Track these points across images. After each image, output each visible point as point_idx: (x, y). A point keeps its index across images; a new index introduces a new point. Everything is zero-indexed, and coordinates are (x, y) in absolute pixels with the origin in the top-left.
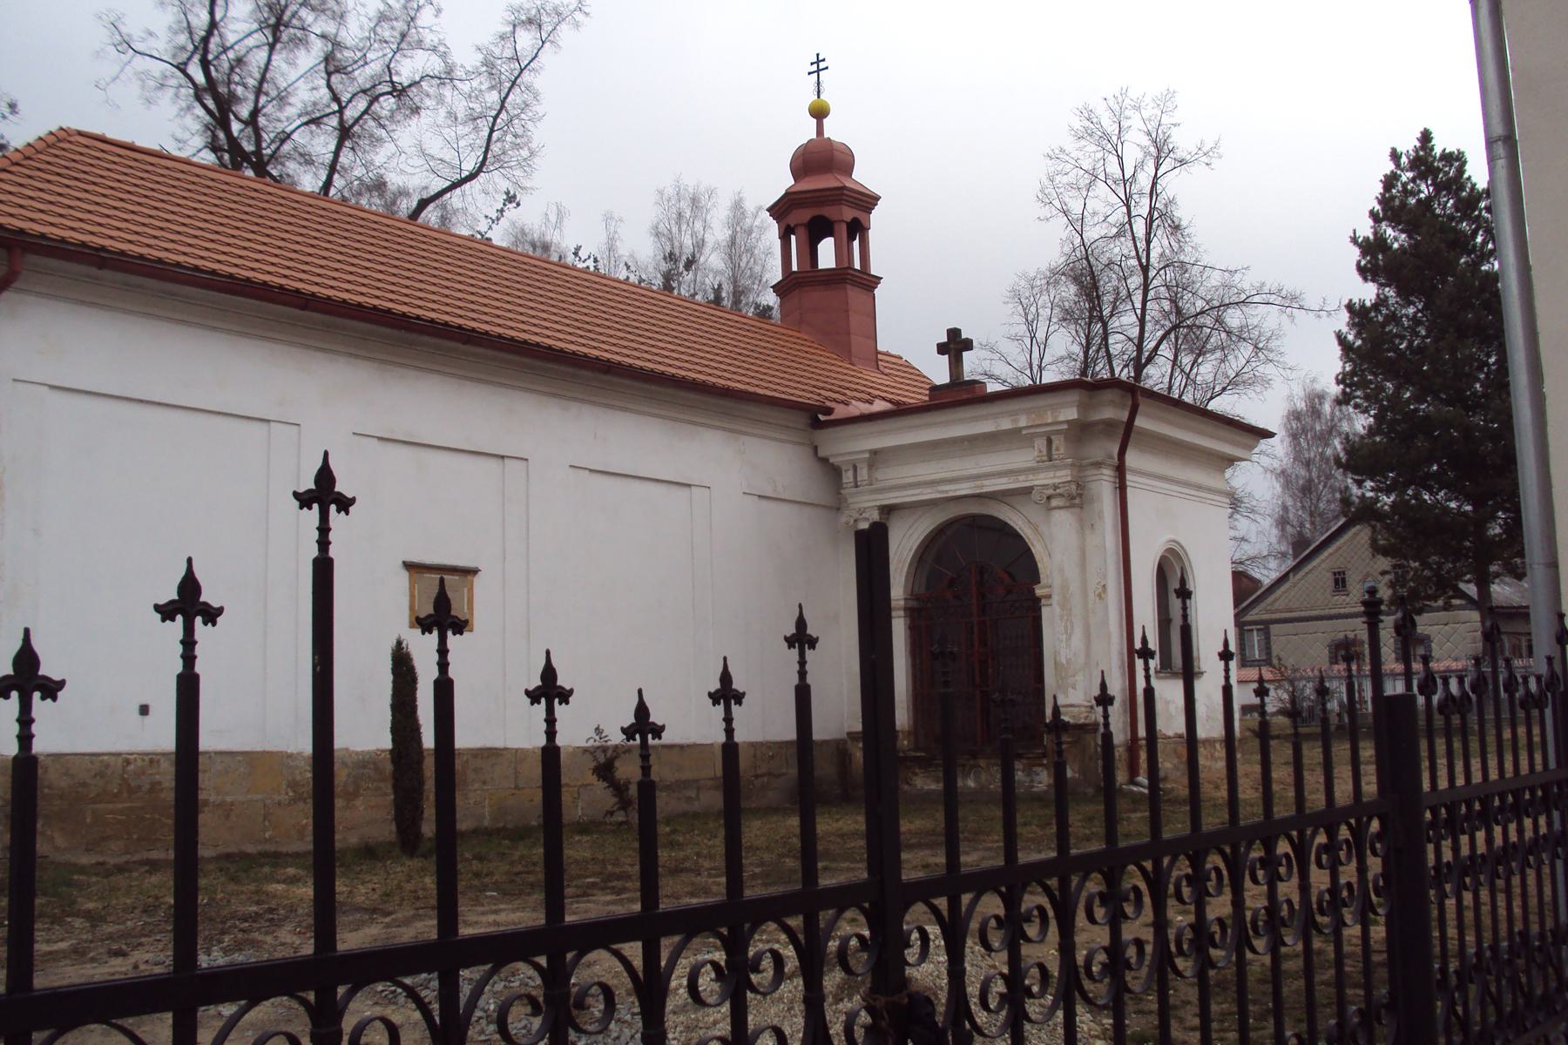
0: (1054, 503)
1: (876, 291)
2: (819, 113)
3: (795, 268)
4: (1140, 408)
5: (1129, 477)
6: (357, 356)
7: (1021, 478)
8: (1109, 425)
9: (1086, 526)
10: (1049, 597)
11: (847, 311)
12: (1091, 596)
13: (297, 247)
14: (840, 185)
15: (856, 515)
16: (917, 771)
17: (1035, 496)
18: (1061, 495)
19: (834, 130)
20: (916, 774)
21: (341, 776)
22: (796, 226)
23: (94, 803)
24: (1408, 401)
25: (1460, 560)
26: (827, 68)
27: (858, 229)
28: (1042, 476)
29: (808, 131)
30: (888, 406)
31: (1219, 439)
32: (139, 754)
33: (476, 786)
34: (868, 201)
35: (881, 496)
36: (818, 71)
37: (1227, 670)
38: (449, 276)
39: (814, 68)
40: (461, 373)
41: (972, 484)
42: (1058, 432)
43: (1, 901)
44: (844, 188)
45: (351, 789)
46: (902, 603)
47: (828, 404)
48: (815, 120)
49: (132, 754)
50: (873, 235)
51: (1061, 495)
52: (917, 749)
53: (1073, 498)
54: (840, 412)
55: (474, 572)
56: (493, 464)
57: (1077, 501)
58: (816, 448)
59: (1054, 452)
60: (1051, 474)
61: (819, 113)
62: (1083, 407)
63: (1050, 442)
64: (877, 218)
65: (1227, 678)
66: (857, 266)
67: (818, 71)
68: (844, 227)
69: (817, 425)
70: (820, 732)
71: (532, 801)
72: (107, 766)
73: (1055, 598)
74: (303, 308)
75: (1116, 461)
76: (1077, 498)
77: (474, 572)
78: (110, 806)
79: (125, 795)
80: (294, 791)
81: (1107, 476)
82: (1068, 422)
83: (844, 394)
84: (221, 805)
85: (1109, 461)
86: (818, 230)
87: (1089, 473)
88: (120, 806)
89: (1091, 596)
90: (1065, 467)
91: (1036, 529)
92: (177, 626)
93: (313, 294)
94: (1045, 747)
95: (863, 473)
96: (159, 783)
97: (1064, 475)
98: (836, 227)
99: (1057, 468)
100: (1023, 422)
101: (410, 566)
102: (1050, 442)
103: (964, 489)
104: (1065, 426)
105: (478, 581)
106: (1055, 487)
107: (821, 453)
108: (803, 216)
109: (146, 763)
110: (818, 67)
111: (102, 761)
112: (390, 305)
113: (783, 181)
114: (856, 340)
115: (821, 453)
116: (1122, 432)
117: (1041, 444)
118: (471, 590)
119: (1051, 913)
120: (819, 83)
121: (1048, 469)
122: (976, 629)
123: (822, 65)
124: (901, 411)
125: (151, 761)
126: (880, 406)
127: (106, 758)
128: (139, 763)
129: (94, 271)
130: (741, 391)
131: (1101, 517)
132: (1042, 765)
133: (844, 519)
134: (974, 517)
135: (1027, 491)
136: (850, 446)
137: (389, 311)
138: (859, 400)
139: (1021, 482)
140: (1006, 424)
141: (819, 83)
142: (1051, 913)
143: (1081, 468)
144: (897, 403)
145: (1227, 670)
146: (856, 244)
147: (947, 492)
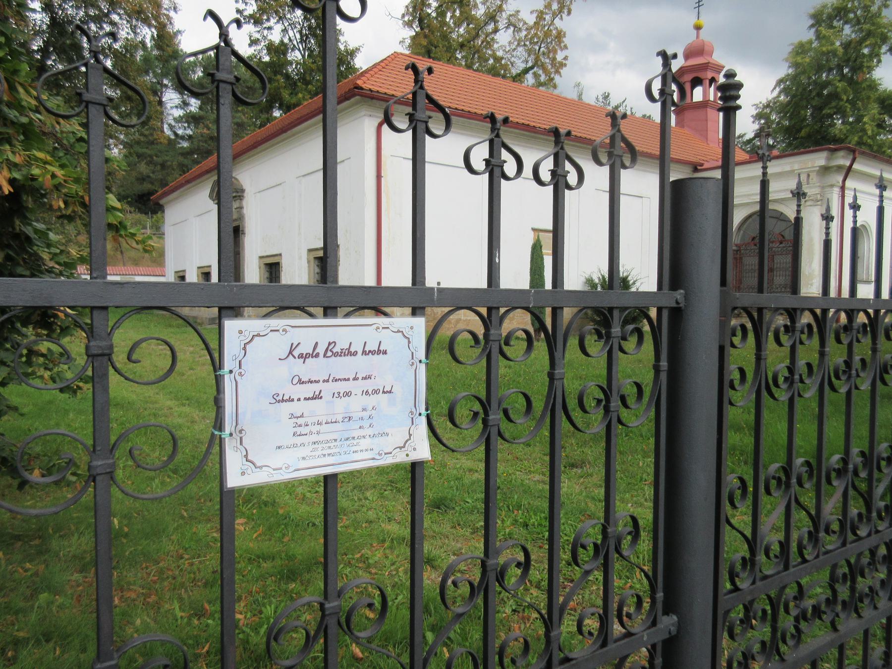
2: (698, 28)
6: (526, 147)
8: (839, 168)
11: (707, 120)
25: (847, 46)
36: (699, 6)
48: (695, 32)
54: (706, 165)
57: (819, 203)
59: (810, 180)
61: (698, 28)
62: (828, 159)
63: (809, 175)
67: (699, 6)
68: (707, 82)
71: (415, 449)
84: (466, 320)
87: (826, 190)
98: (704, 81)
100: (796, 167)
102: (809, 175)
116: (845, 171)
119: (815, 329)
123: (701, 4)
140: (787, 168)
142: (815, 329)
143: (823, 188)
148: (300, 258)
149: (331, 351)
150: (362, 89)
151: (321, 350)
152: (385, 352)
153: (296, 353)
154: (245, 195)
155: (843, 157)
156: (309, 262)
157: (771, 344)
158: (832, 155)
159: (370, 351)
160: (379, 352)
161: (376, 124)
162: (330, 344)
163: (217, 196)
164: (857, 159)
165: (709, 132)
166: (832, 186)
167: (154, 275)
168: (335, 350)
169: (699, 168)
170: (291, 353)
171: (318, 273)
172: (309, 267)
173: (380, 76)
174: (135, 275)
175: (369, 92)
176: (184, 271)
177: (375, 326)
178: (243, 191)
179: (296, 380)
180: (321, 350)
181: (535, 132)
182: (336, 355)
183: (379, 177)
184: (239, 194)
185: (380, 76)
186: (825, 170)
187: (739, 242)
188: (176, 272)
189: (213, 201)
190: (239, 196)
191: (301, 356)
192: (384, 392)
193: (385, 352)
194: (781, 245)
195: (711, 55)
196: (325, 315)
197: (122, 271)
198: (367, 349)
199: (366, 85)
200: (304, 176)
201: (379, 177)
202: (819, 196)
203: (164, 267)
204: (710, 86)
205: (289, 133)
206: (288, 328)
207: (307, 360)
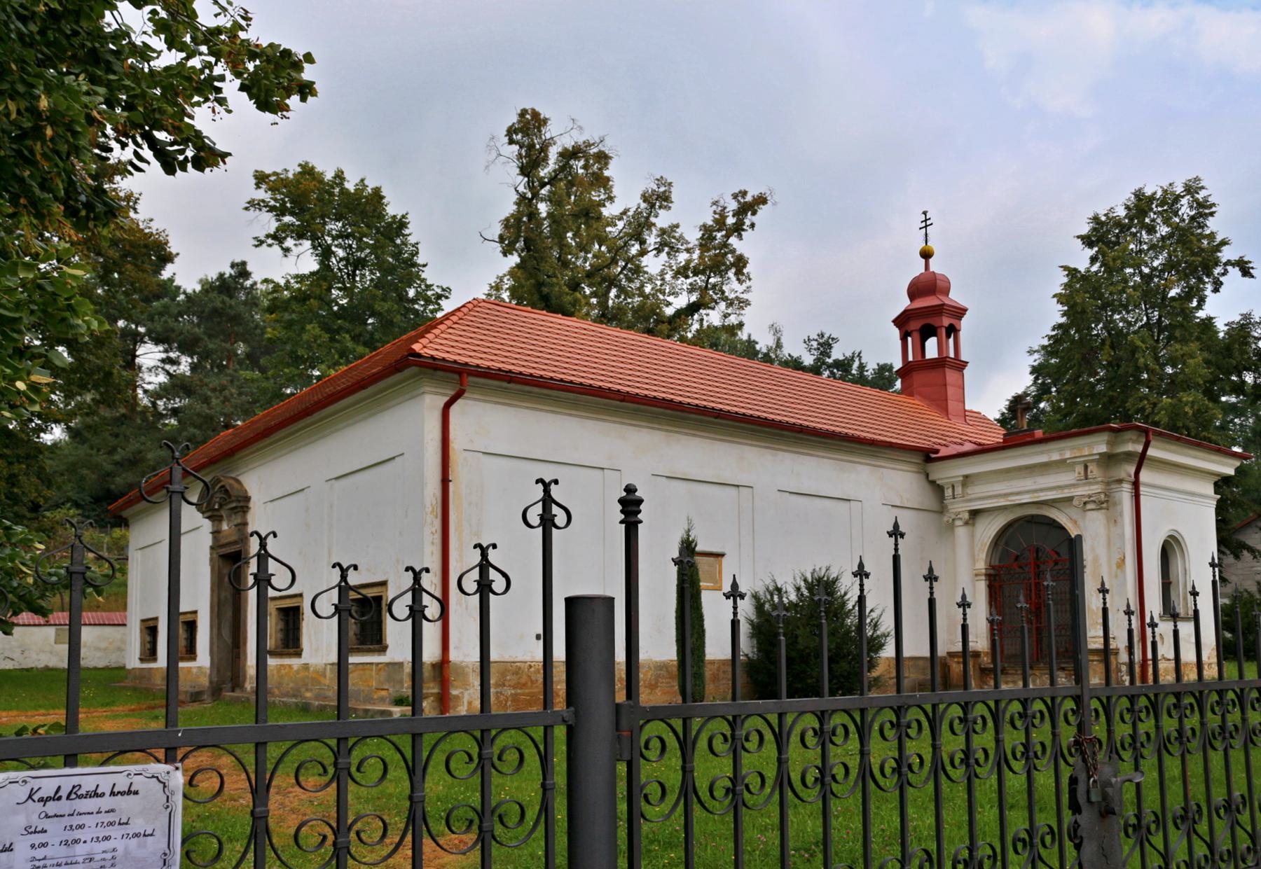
0: (1089, 506)
1: (965, 371)
2: (926, 255)
5: (1142, 488)
7: (1066, 491)
8: (1128, 456)
9: (1115, 521)
11: (945, 385)
12: (1114, 567)
13: (614, 364)
14: (940, 303)
15: (953, 517)
17: (1075, 502)
18: (1094, 502)
19: (936, 266)
21: (644, 676)
27: (953, 330)
28: (1080, 489)
29: (918, 267)
31: (1213, 462)
34: (960, 312)
36: (926, 226)
37: (1130, 620)
39: (924, 224)
40: (712, 435)
41: (1031, 495)
42: (1092, 461)
44: (944, 305)
45: (653, 683)
46: (984, 571)
47: (936, 447)
48: (923, 261)
50: (963, 335)
51: (1094, 502)
53: (1103, 503)
54: (944, 452)
55: (722, 555)
56: (733, 491)
57: (1104, 505)
58: (927, 475)
60: (1087, 488)
61: (926, 255)
62: (1110, 443)
63: (1086, 467)
64: (965, 324)
65: (1130, 625)
66: (952, 355)
67: (926, 226)
70: (941, 651)
72: (520, 668)
74: (622, 401)
75: (1133, 478)
76: (1105, 503)
77: (722, 555)
79: (529, 684)
81: (1127, 488)
82: (1100, 454)
85: (1129, 479)
90: (1097, 483)
91: (1075, 522)
92: (858, 579)
93: (628, 392)
95: (959, 490)
97: (1096, 488)
98: (939, 330)
99: (1091, 484)
100: (1068, 455)
102: (1086, 467)
103: (1026, 499)
104: (1097, 457)
105: (725, 560)
106: (1090, 496)
107: (930, 479)
108: (915, 325)
110: (926, 223)
112: (672, 397)
113: (903, 303)
114: (952, 405)
115: (930, 479)
117: (1080, 469)
118: (720, 565)
121: (1085, 484)
122: (1033, 588)
123: (928, 222)
124: (982, 450)
126: (968, 447)
129: (505, 384)
130: (882, 441)
131: (1121, 514)
133: (945, 519)
134: (1033, 516)
135: (1070, 499)
136: (948, 473)
137: (672, 401)
138: (955, 443)
139: (1066, 493)
140: (1056, 457)
141: (926, 234)
143: (1108, 484)
144: (980, 444)
145: (1130, 620)
146: (951, 341)
149: (74, 794)
150: (419, 355)
151: (64, 793)
152: (136, 793)
153: (36, 797)
154: (251, 505)
155: (1134, 442)
157: (1209, 715)
158: (1116, 437)
159: (119, 792)
160: (129, 792)
161: (442, 405)
162: (74, 787)
163: (209, 509)
164: (1152, 443)
165: (950, 402)
166: (1120, 481)
167: (109, 625)
168: (79, 793)
170: (30, 797)
173: (476, 314)
175: (431, 361)
177: (126, 773)
178: (248, 499)
179: (43, 815)
180: (64, 793)
181: (682, 411)
182: (80, 797)
183: (445, 481)
184: (242, 504)
185: (476, 314)
186: (1109, 460)
187: (997, 563)
188: (143, 621)
189: (203, 513)
190: (242, 507)
191: (41, 800)
192: (120, 824)
193: (136, 793)
194: (1056, 567)
195: (946, 291)
196: (66, 765)
197: (58, 618)
198: (116, 790)
199: (426, 350)
200: (337, 478)
201: (445, 481)
202: (1103, 496)
203: (125, 608)
204: (948, 336)
205: (316, 416)
206: (28, 779)
207: (48, 803)
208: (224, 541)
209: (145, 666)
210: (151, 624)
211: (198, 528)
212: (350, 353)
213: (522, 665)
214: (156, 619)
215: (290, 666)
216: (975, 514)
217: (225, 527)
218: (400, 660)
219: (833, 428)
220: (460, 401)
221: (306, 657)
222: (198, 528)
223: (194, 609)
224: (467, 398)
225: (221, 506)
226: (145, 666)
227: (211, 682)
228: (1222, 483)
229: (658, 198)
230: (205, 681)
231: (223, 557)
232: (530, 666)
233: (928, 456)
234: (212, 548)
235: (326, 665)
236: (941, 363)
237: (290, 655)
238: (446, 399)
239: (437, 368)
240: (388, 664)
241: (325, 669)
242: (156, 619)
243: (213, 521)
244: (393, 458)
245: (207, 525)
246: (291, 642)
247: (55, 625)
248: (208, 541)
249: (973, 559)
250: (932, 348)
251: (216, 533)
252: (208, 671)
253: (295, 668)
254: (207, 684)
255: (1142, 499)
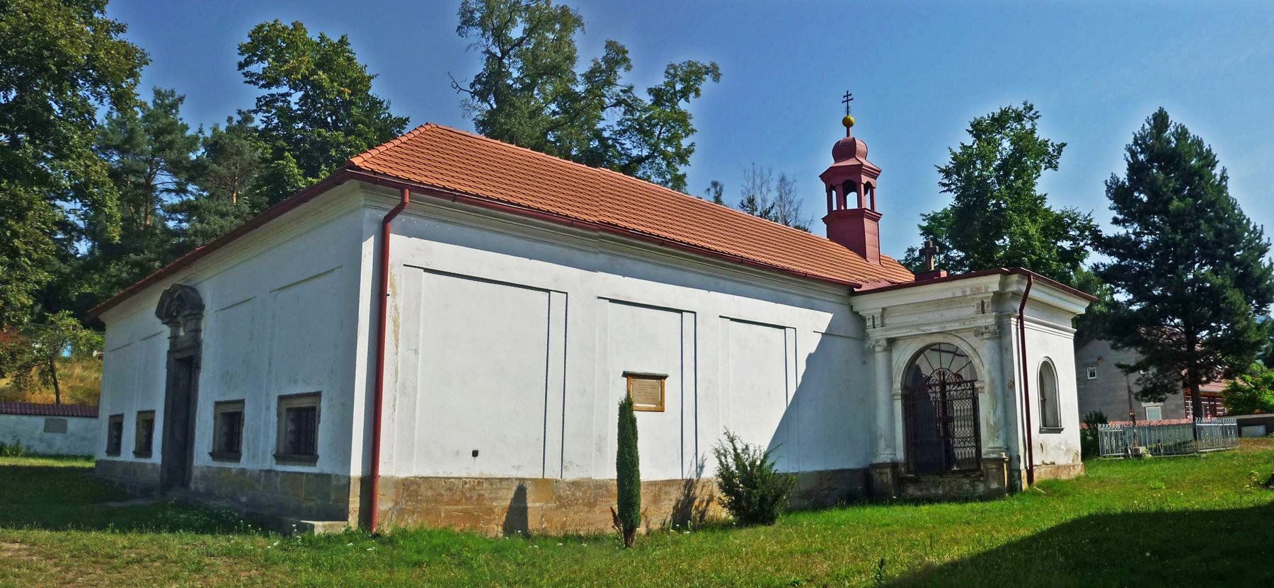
3: (835, 208)
4: (1032, 285)
10: (983, 388)
12: (1007, 388)
16: (909, 484)
20: (908, 486)
22: (836, 185)
23: (446, 505)
24: (1192, 290)
26: (852, 99)
30: (889, 284)
32: (471, 478)
33: (666, 502)
35: (888, 333)
36: (848, 101)
38: (634, 207)
39: (846, 99)
43: (1, 136)
45: (592, 501)
49: (467, 478)
52: (909, 472)
55: (665, 377)
58: (852, 306)
61: (847, 123)
67: (848, 101)
69: (853, 294)
73: (987, 389)
74: (571, 225)
77: (665, 377)
78: (455, 507)
79: (464, 501)
80: (560, 502)
83: (865, 277)
86: (851, 186)
88: (460, 507)
89: (1007, 388)
94: (982, 472)
95: (878, 322)
96: (483, 495)
101: (626, 375)
103: (935, 329)
105: (667, 381)
107: (855, 310)
109: (476, 483)
110: (848, 98)
111: (451, 482)
114: (870, 249)
115: (855, 310)
120: (848, 108)
123: (850, 98)
125: (479, 482)
126: (884, 284)
127: (453, 480)
128: (472, 483)
132: (980, 481)
141: (848, 108)
144: (893, 283)
147: (925, 331)
148: (268, 408)
150: (359, 168)
156: (279, 415)
163: (165, 314)
169: (856, 290)
171: (291, 431)
172: (279, 422)
174: (68, 416)
176: (122, 416)
178: (201, 307)
204: (866, 193)
208: (179, 347)
209: (110, 458)
210: (118, 420)
211: (159, 333)
212: (111, 92)
213: (456, 482)
214: (153, 412)
215: (229, 469)
216: (891, 342)
217: (182, 333)
218: (330, 472)
219: (771, 262)
220: (399, 216)
221: (245, 463)
222: (159, 333)
223: (120, 413)
224: (407, 214)
225: (178, 313)
226: (110, 458)
227: (162, 479)
228: (1078, 321)
229: (616, 57)
230: (157, 476)
231: (179, 360)
232: (466, 483)
233: (851, 290)
234: (169, 352)
235: (261, 471)
236: (860, 213)
237: (230, 459)
238: (384, 214)
239: (373, 181)
240: (317, 475)
241: (260, 475)
242: (153, 412)
243: (171, 327)
244: (333, 270)
245: (167, 331)
246: (229, 444)
247: (45, 415)
248: (166, 346)
249: (891, 381)
250: (852, 201)
251: (174, 338)
252: (160, 468)
253: (234, 472)
254: (158, 480)
255: (1026, 330)
